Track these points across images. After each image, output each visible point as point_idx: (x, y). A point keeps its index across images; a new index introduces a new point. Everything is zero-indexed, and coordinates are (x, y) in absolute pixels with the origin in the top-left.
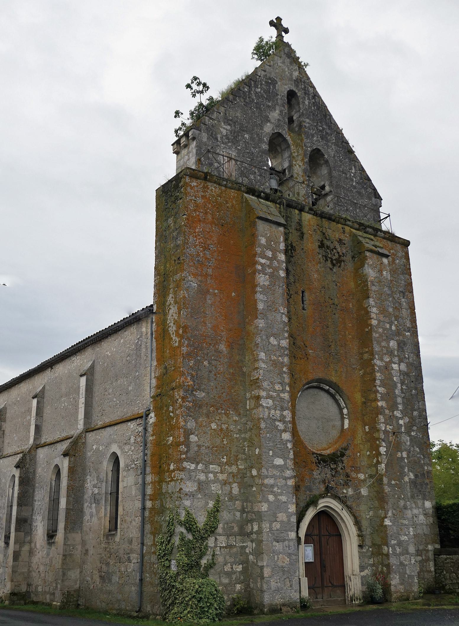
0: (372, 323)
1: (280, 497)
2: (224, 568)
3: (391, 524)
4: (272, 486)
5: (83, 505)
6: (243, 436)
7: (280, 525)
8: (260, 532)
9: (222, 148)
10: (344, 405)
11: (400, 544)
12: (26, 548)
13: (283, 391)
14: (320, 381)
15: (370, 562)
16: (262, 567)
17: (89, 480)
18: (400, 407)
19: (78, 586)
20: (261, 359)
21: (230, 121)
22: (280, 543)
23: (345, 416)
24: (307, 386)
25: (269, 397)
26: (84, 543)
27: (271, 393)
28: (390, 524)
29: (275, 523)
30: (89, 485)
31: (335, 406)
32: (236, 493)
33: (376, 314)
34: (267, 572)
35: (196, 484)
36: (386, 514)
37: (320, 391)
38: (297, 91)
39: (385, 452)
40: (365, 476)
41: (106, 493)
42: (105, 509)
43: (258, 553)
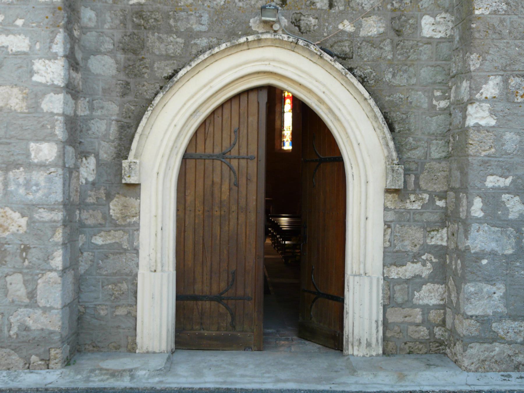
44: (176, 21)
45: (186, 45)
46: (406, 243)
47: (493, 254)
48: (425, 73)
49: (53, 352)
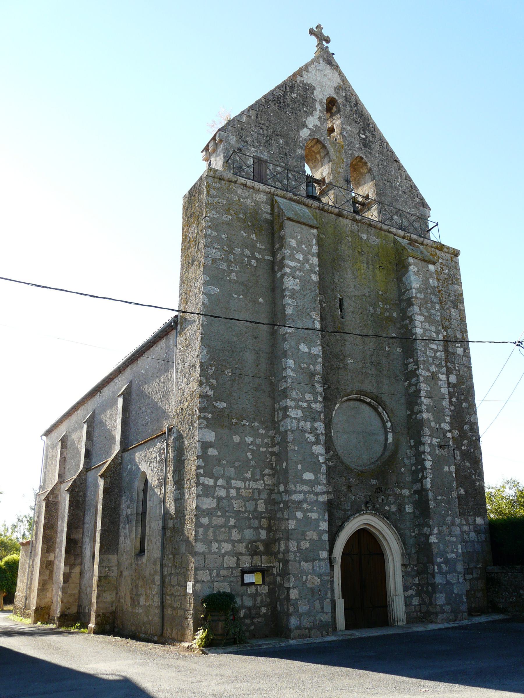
0: (417, 332)
1: (310, 514)
2: (247, 590)
3: (437, 541)
4: (300, 502)
5: (119, 526)
6: (270, 450)
7: (309, 544)
8: (287, 551)
9: (252, 151)
10: (388, 419)
11: (447, 561)
12: (77, 570)
13: (315, 401)
14: (360, 392)
15: (415, 582)
16: (288, 589)
17: (124, 501)
18: (448, 419)
19: (114, 608)
20: (289, 367)
21: (262, 124)
22: (309, 563)
23: (388, 430)
24: (346, 398)
25: (297, 407)
26: (119, 564)
27: (300, 403)
28: (436, 541)
29: (304, 542)
30: (124, 505)
31: (378, 418)
32: (262, 511)
33: (422, 322)
34: (294, 594)
35: (215, 500)
36: (431, 531)
37: (362, 403)
38: (337, 98)
39: (431, 466)
40: (410, 491)
41: (137, 514)
42: (136, 530)
43: (285, 573)
44: (341, 505)
45: (345, 514)
46: (408, 583)
47: (441, 583)
48: (408, 524)
49: (330, 629)
